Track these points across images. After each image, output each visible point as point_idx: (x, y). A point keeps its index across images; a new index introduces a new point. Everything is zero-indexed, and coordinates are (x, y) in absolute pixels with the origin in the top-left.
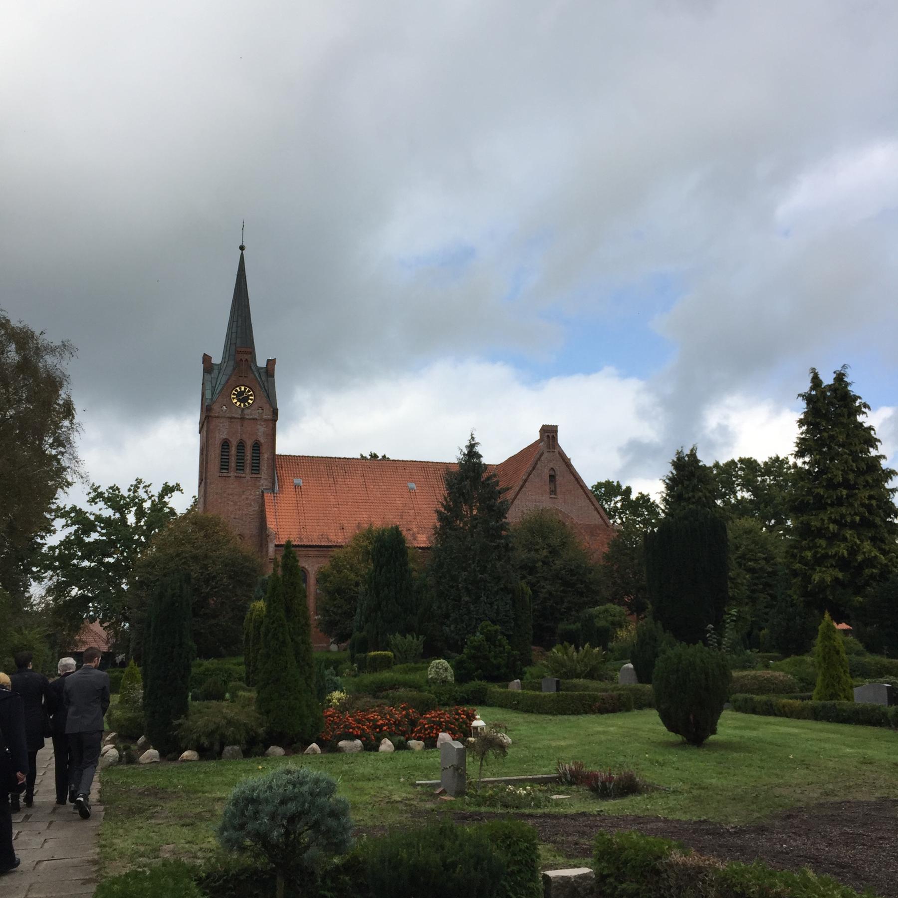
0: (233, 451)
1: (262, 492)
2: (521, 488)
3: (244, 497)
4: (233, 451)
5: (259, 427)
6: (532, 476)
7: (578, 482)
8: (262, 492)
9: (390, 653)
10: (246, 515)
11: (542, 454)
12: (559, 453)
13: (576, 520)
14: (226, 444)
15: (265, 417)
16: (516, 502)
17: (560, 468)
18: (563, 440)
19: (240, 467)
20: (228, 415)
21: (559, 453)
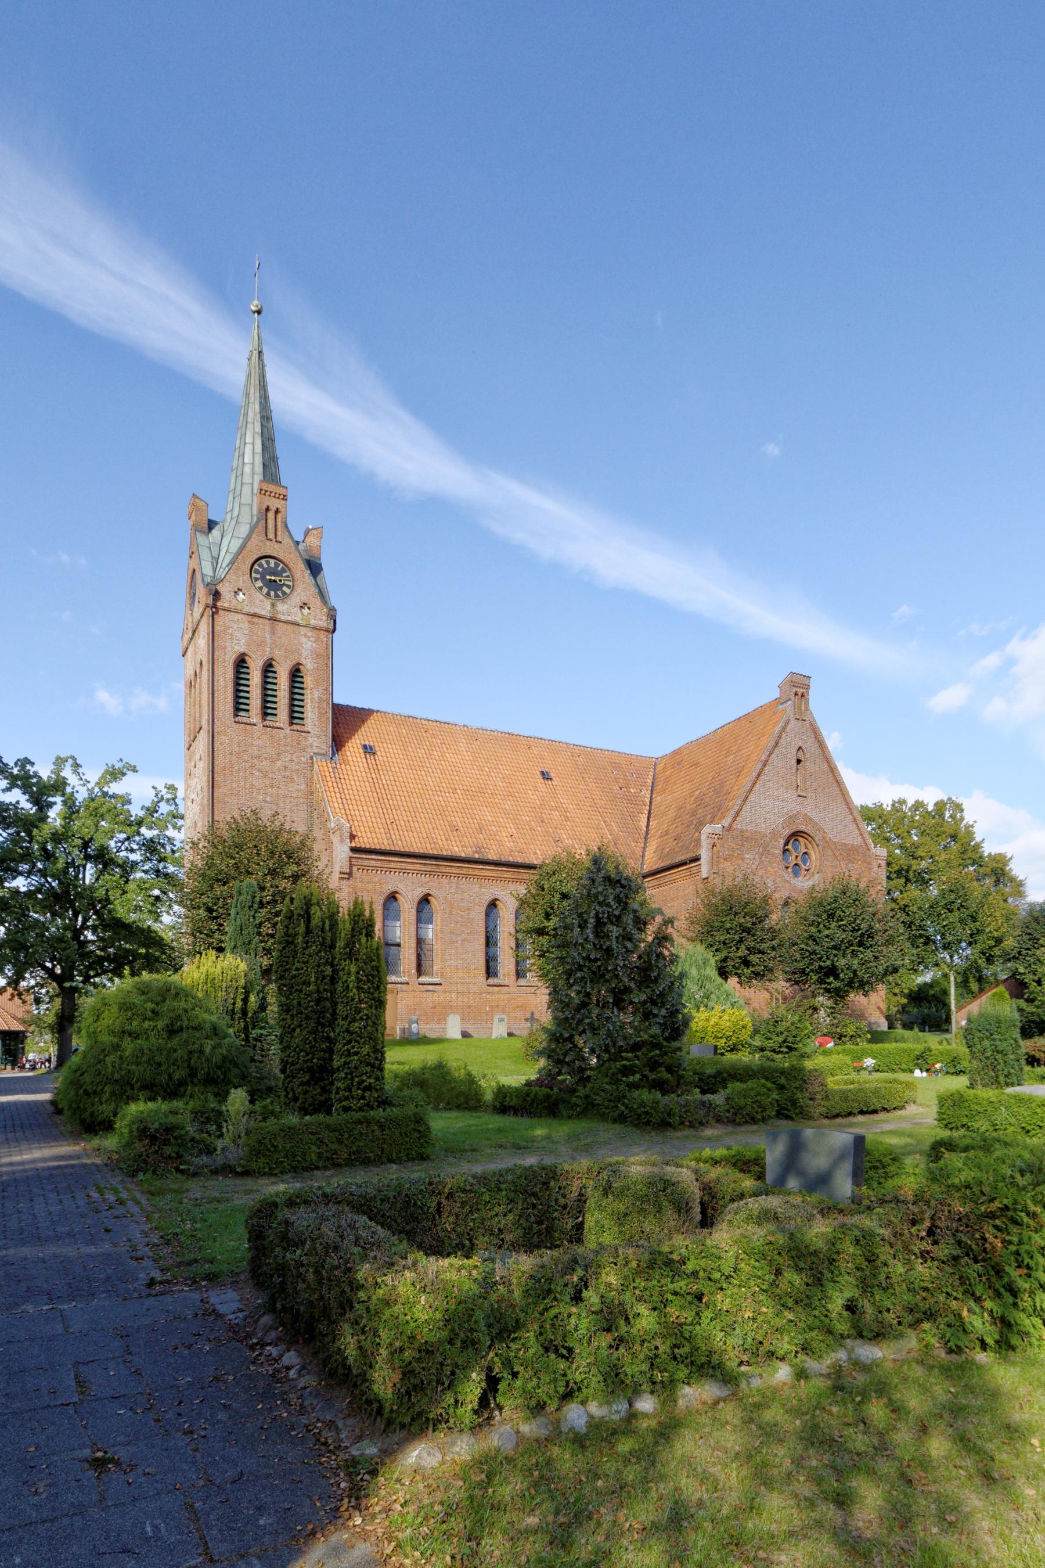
0: (255, 678)
1: (312, 758)
2: (759, 775)
3: (279, 764)
4: (255, 678)
5: (303, 640)
6: (773, 756)
7: (834, 775)
8: (312, 758)
9: (268, 577)
10: (285, 796)
11: (788, 722)
12: (811, 724)
13: (830, 835)
14: (241, 663)
15: (313, 622)
16: (503, 845)
17: (810, 746)
18: (818, 704)
19: (267, 711)
20: (247, 609)
21: (811, 724)
